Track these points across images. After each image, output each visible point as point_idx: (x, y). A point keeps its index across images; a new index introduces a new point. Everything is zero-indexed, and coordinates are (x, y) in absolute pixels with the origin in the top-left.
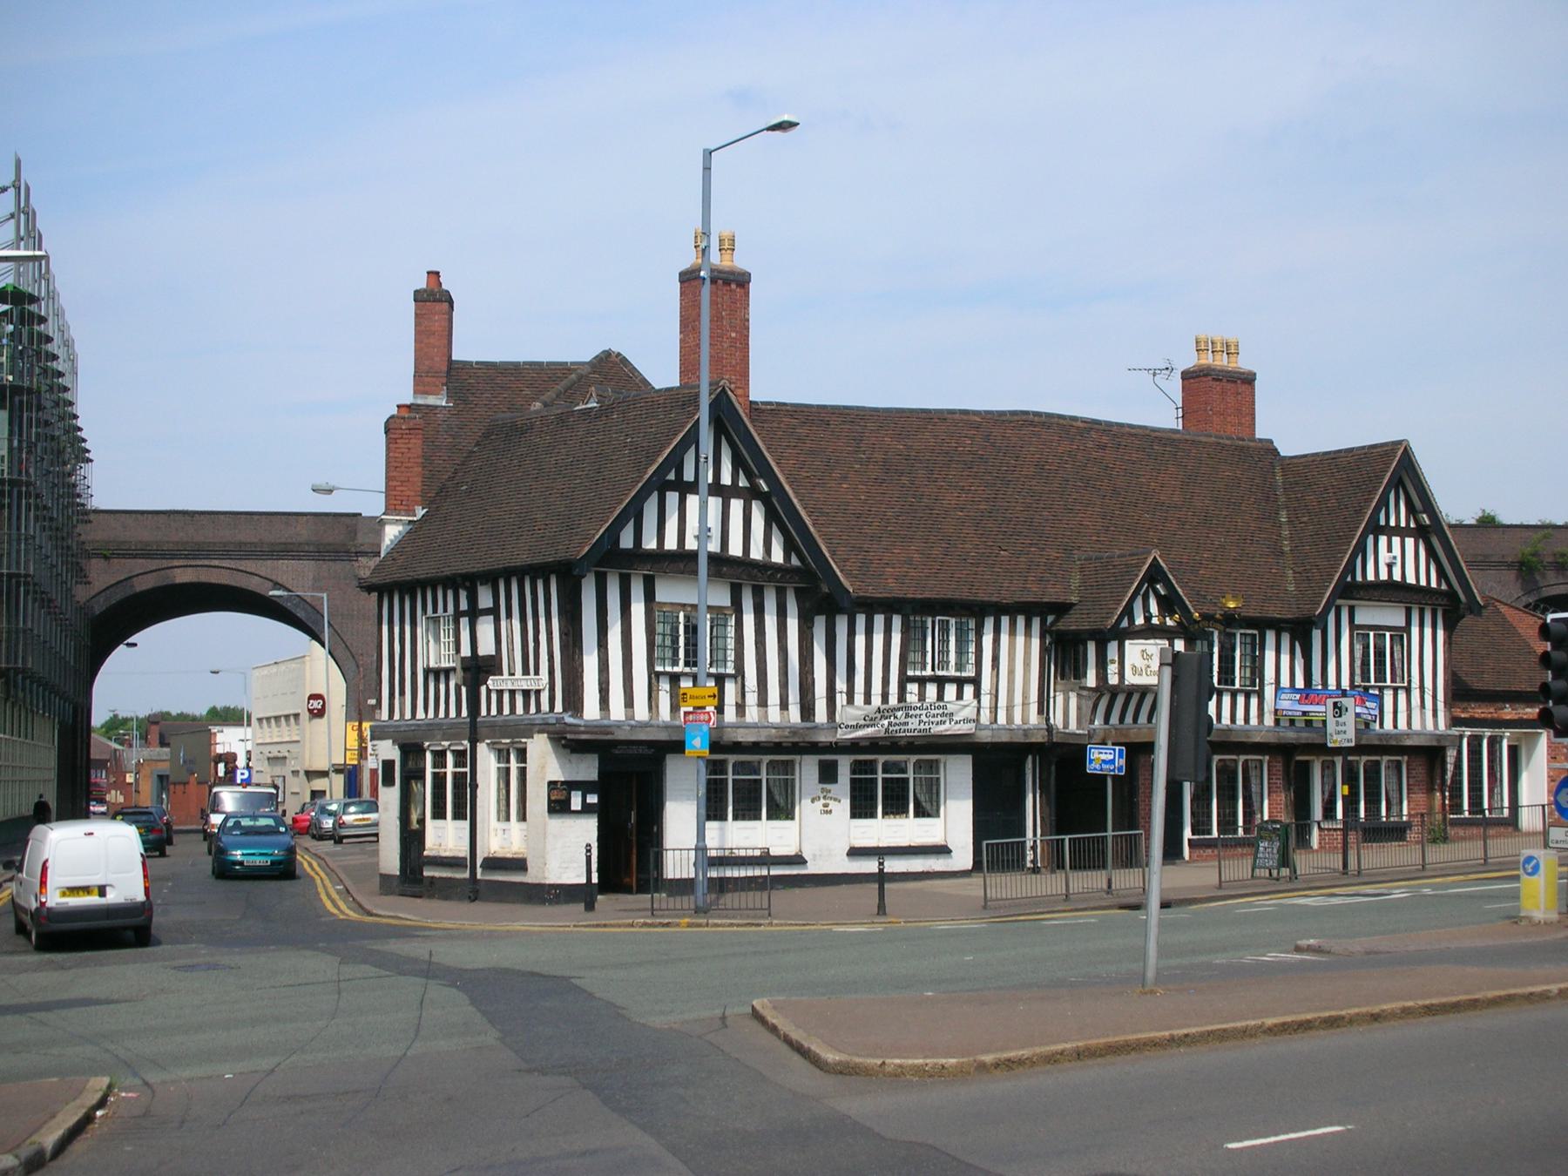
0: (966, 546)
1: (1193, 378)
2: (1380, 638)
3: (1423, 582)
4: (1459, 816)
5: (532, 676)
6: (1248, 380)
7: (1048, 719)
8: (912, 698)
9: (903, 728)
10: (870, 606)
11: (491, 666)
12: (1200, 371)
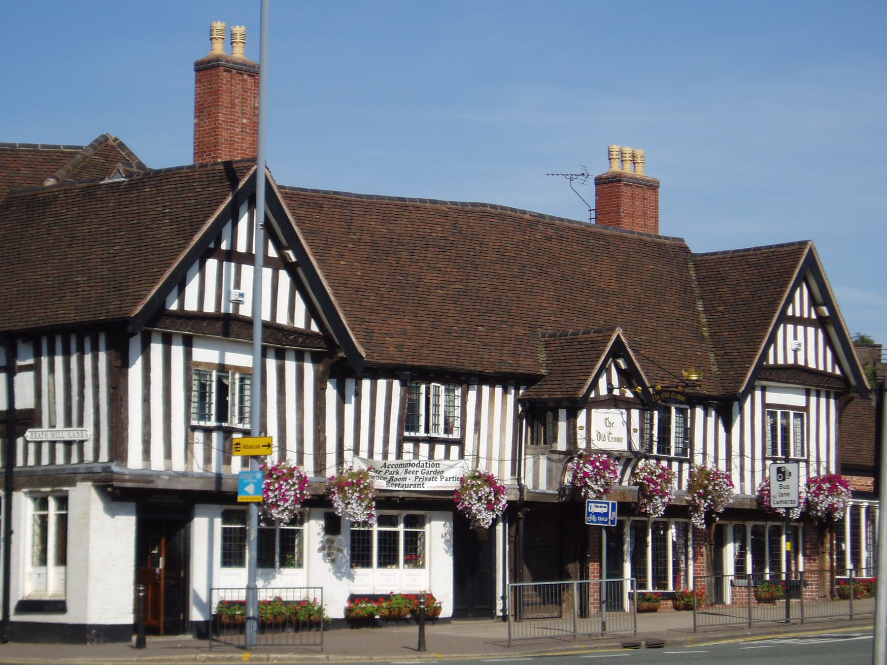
0: (449, 321)
1: (605, 183)
2: (785, 416)
4: (843, 577)
5: (75, 427)
6: (653, 186)
7: (519, 480)
8: (407, 457)
9: (402, 483)
10: (375, 372)
11: (31, 419)
12: (613, 178)
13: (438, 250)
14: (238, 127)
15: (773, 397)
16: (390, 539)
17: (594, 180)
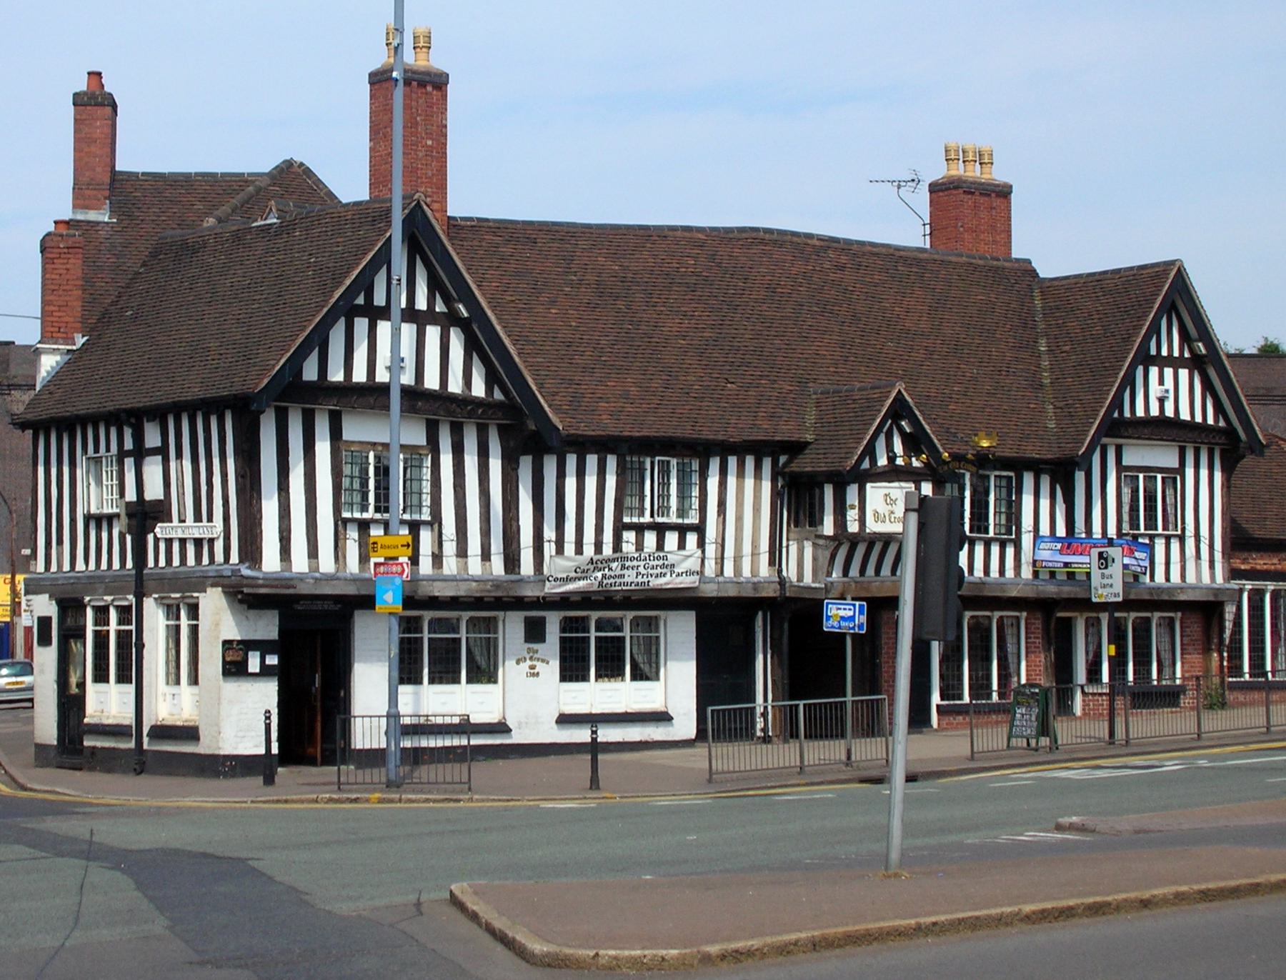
2: (1150, 480)
3: (1199, 419)
4: (1238, 679)
5: (205, 523)
6: (1004, 192)
7: (780, 571)
9: (618, 581)
10: (582, 446)
11: (159, 512)
13: (686, 289)
14: (421, 151)
15: (1133, 457)
16: (572, 657)
17: (927, 185)
